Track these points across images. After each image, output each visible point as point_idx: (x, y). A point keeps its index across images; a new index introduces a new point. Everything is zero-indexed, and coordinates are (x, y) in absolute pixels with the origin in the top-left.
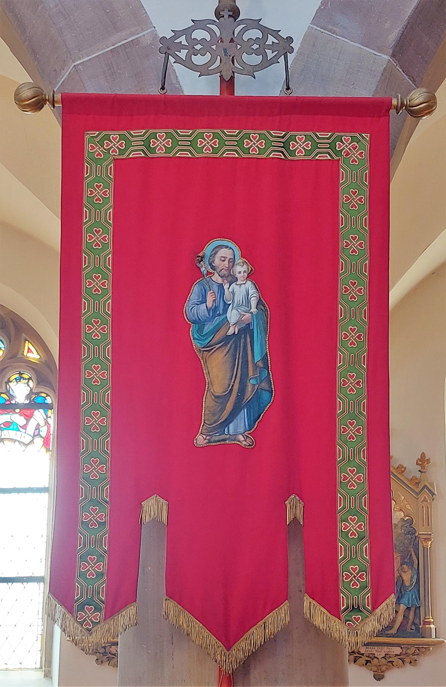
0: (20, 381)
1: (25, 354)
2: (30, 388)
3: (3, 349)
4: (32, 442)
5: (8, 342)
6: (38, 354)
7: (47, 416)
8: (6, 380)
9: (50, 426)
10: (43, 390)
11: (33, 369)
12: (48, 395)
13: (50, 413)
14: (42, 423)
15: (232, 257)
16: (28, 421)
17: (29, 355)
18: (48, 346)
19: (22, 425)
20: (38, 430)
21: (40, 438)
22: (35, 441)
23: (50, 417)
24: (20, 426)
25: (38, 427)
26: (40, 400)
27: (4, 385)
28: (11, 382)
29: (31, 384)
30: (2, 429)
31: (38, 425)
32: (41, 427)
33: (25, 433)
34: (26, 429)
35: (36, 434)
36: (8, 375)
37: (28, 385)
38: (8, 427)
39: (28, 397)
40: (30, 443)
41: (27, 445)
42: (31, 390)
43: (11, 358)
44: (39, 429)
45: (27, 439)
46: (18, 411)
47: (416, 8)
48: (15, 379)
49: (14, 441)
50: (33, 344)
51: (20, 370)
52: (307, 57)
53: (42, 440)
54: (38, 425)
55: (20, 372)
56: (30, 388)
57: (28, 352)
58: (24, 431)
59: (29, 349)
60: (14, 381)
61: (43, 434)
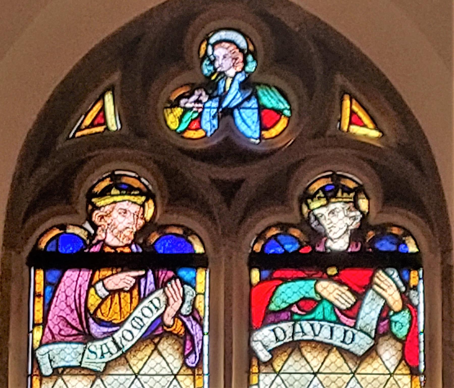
0: (335, 196)
1: (345, 128)
2: (362, 213)
3: (287, 113)
4: (372, 352)
5: (303, 91)
6: (376, 127)
7: (406, 284)
8: (299, 192)
9: (417, 311)
10: (397, 219)
11: (373, 165)
12: (408, 233)
13: (414, 277)
14: (395, 301)
15: (86, 233)
16: (360, 298)
17: (355, 129)
18: (411, 105)
19: (343, 307)
20: (386, 321)
21: (392, 342)
22: (381, 350)
23: (415, 288)
24: (340, 310)
25: (386, 314)
26: (385, 246)
27: (295, 204)
28: (312, 197)
29: (363, 204)
30: (296, 317)
31: (386, 307)
32: (396, 313)
33: (354, 327)
34: (355, 318)
35: (381, 330)
36: (305, 180)
37: (357, 207)
38: (309, 313)
39: (356, 235)
40: (368, 353)
41: (360, 359)
42: (365, 217)
43: (315, 137)
44: (388, 317)
45: (362, 343)
46: (332, 271)
47: (366, 57)
48: (323, 189)
49: (327, 347)
50: (365, 103)
51: (335, 167)
52: (328, 75)
53: (399, 346)
54: (386, 307)
55: (334, 173)
56: (362, 213)
57: (351, 123)
58: (351, 322)
59: (352, 112)
60: (321, 194)
61: (401, 331)
